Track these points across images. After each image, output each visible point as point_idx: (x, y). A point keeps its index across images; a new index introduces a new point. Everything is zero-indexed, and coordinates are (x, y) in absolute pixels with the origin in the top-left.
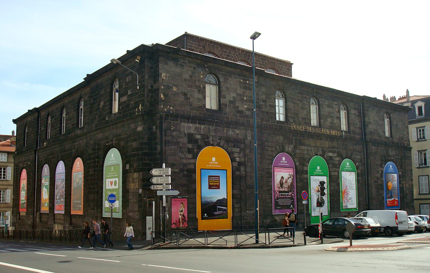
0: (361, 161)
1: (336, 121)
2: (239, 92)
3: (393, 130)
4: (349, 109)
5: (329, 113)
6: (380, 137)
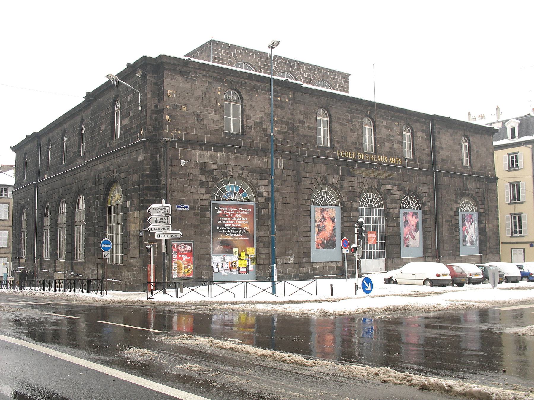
0: (429, 196)
1: (396, 146)
2: (267, 111)
3: (472, 157)
4: (414, 131)
5: (388, 136)
6: (455, 166)
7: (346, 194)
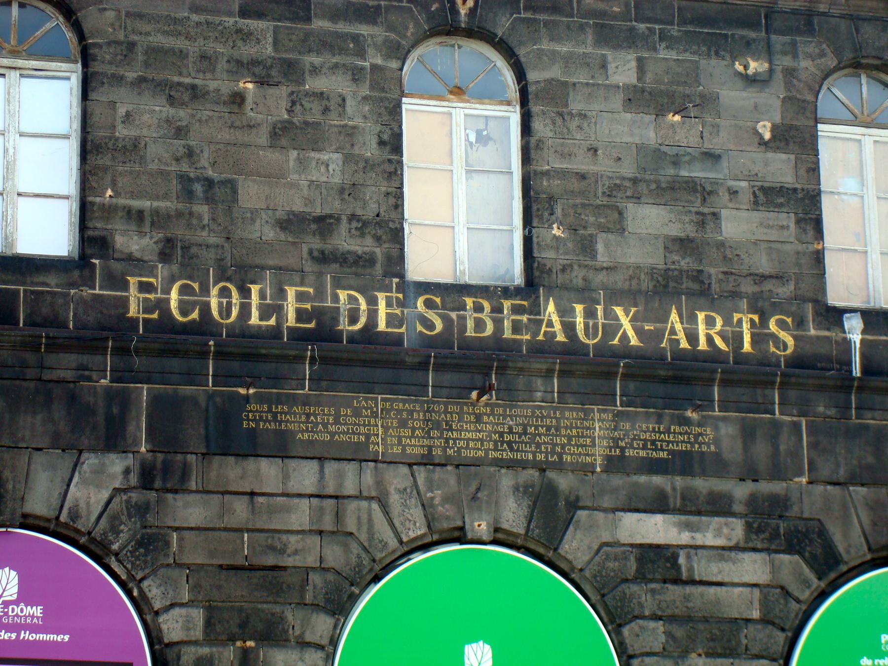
7: (196, 588)
